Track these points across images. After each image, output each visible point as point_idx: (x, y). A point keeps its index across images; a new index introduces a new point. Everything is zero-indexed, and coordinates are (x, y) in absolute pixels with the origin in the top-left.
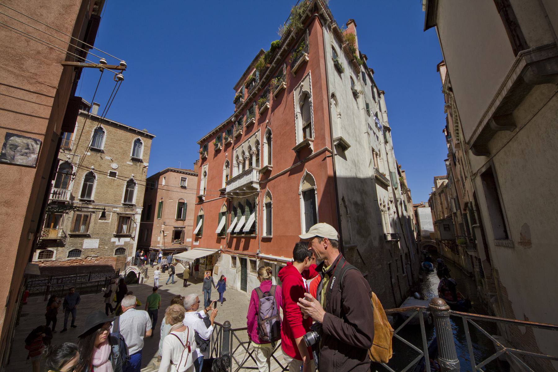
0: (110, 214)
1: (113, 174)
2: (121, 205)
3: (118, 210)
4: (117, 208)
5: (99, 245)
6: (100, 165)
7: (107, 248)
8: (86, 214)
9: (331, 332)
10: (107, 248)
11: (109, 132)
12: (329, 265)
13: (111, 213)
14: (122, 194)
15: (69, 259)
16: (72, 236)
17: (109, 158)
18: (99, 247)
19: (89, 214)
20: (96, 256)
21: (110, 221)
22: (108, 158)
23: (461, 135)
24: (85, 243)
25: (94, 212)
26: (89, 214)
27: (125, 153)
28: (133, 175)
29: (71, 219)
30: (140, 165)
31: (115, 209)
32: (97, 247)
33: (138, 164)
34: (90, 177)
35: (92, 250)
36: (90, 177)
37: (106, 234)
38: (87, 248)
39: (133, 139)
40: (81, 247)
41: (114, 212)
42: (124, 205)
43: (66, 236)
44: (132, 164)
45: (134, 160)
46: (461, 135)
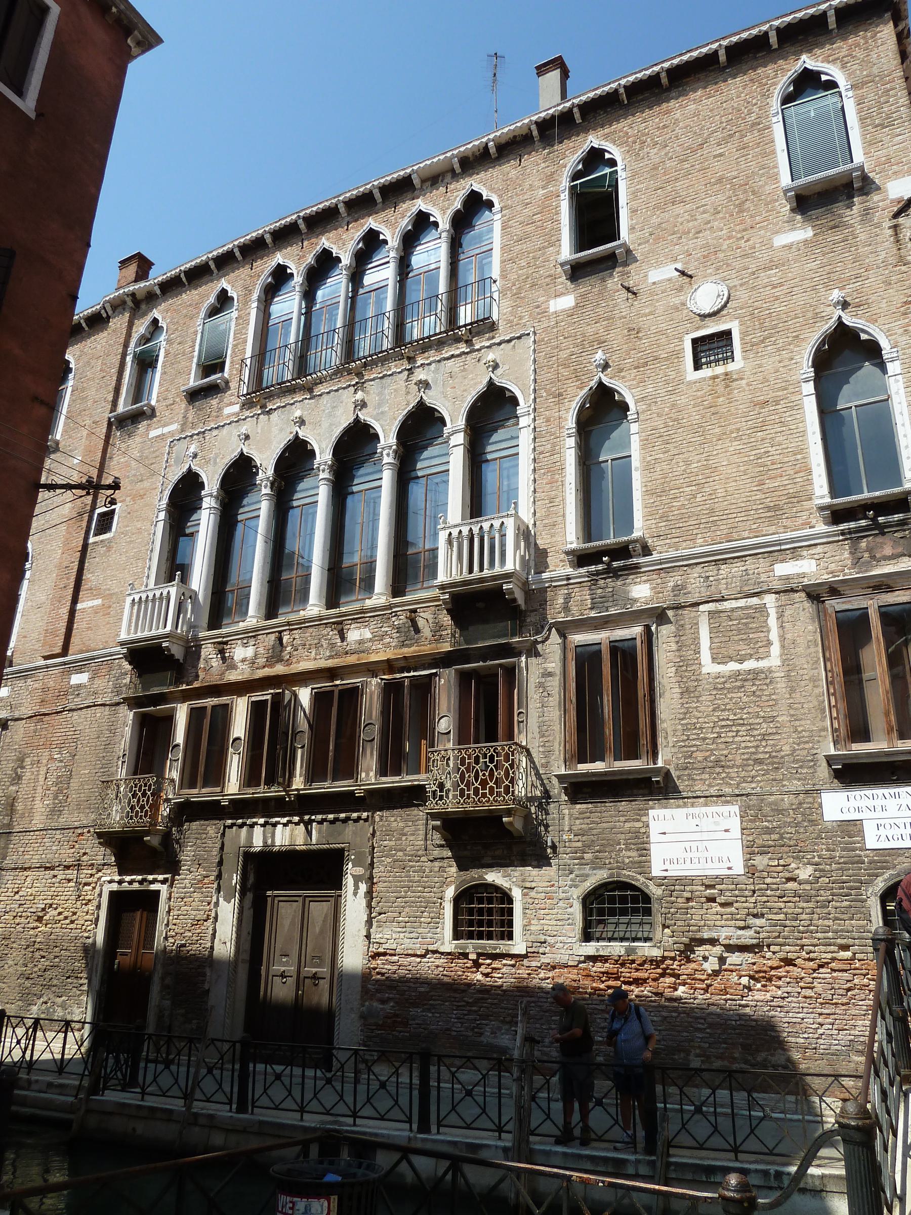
0: (762, 610)
1: (712, 347)
2: (822, 528)
3: (806, 568)
4: (795, 553)
5: (750, 850)
6: (634, 332)
7: (805, 873)
8: (621, 633)
9: (249, 505)
10: (805, 873)
11: (635, 147)
12: (288, 663)
13: (770, 600)
14: (802, 450)
15: (591, 948)
16: (581, 790)
17: (668, 272)
18: (751, 871)
19: (636, 630)
20: (747, 936)
21: (774, 660)
22: (663, 273)
23: (28, 1052)
24: (655, 829)
25: (660, 616)
26: (636, 630)
27: (744, 195)
28: (836, 295)
29: (554, 684)
30: (866, 213)
31: (783, 569)
32: (739, 869)
33: (853, 213)
34: (602, 411)
35: (712, 890)
36: (602, 411)
37: (775, 763)
38: (675, 871)
39: (766, 95)
40: (643, 866)
41: (788, 590)
42: (837, 516)
43: (547, 794)
44: (808, 233)
45: (807, 202)
46: (28, 1052)
